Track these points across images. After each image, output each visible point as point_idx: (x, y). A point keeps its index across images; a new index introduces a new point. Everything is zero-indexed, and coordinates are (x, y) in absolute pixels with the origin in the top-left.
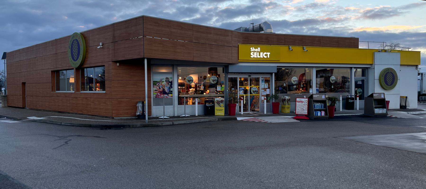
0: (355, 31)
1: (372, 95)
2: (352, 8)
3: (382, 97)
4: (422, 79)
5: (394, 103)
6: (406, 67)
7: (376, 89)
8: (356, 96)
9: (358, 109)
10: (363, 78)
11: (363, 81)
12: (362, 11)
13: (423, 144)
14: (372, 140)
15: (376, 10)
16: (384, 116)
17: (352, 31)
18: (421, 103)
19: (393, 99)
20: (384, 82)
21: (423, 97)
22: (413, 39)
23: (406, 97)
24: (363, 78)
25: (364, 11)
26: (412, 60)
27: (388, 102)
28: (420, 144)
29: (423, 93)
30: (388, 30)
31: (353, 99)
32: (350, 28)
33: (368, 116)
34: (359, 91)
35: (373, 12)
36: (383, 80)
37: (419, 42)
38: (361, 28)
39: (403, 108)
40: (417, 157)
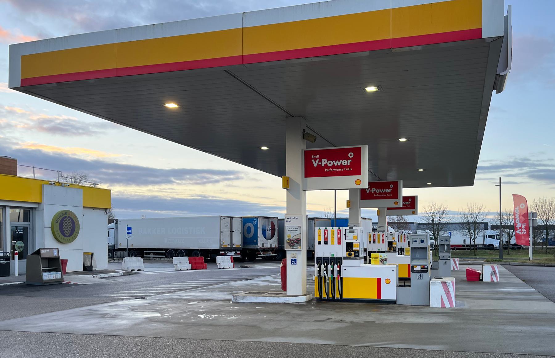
0: (24, 147)
1: (39, 251)
2: (18, 110)
3: (55, 254)
4: (117, 228)
5: (74, 264)
6: (92, 210)
7: (45, 241)
8: (14, 254)
9: (17, 274)
10: (26, 224)
11: (25, 229)
12: (35, 118)
13: (102, 320)
14: (27, 324)
15: (58, 121)
16: (58, 284)
17: (17, 147)
18: (116, 261)
19: (72, 255)
20: (59, 232)
21: (119, 253)
22: (110, 171)
23: (92, 254)
24: (26, 224)
25: (39, 119)
26: (101, 203)
27: (64, 262)
28: (97, 320)
29: (119, 247)
30: (75, 154)
31: (8, 258)
32: (15, 141)
33: (33, 285)
34: (19, 245)
35: (53, 124)
36: (57, 228)
37: (118, 177)
38: (33, 145)
39: (87, 269)
40: (88, 341)
